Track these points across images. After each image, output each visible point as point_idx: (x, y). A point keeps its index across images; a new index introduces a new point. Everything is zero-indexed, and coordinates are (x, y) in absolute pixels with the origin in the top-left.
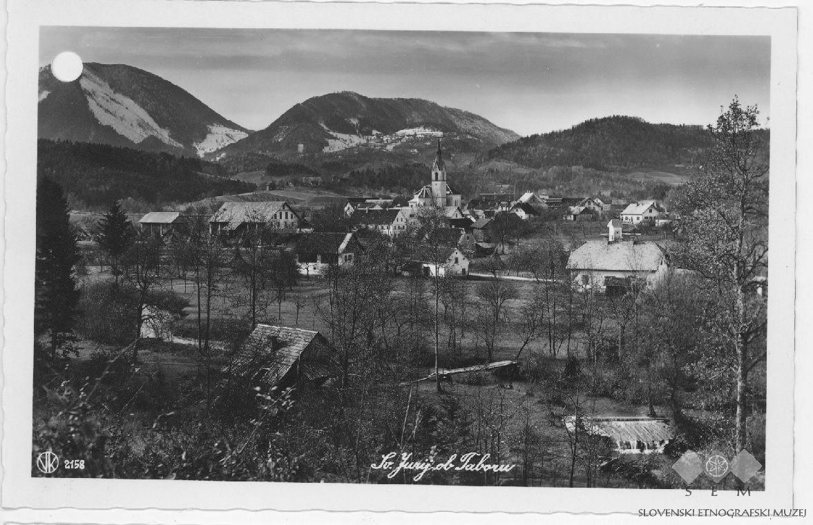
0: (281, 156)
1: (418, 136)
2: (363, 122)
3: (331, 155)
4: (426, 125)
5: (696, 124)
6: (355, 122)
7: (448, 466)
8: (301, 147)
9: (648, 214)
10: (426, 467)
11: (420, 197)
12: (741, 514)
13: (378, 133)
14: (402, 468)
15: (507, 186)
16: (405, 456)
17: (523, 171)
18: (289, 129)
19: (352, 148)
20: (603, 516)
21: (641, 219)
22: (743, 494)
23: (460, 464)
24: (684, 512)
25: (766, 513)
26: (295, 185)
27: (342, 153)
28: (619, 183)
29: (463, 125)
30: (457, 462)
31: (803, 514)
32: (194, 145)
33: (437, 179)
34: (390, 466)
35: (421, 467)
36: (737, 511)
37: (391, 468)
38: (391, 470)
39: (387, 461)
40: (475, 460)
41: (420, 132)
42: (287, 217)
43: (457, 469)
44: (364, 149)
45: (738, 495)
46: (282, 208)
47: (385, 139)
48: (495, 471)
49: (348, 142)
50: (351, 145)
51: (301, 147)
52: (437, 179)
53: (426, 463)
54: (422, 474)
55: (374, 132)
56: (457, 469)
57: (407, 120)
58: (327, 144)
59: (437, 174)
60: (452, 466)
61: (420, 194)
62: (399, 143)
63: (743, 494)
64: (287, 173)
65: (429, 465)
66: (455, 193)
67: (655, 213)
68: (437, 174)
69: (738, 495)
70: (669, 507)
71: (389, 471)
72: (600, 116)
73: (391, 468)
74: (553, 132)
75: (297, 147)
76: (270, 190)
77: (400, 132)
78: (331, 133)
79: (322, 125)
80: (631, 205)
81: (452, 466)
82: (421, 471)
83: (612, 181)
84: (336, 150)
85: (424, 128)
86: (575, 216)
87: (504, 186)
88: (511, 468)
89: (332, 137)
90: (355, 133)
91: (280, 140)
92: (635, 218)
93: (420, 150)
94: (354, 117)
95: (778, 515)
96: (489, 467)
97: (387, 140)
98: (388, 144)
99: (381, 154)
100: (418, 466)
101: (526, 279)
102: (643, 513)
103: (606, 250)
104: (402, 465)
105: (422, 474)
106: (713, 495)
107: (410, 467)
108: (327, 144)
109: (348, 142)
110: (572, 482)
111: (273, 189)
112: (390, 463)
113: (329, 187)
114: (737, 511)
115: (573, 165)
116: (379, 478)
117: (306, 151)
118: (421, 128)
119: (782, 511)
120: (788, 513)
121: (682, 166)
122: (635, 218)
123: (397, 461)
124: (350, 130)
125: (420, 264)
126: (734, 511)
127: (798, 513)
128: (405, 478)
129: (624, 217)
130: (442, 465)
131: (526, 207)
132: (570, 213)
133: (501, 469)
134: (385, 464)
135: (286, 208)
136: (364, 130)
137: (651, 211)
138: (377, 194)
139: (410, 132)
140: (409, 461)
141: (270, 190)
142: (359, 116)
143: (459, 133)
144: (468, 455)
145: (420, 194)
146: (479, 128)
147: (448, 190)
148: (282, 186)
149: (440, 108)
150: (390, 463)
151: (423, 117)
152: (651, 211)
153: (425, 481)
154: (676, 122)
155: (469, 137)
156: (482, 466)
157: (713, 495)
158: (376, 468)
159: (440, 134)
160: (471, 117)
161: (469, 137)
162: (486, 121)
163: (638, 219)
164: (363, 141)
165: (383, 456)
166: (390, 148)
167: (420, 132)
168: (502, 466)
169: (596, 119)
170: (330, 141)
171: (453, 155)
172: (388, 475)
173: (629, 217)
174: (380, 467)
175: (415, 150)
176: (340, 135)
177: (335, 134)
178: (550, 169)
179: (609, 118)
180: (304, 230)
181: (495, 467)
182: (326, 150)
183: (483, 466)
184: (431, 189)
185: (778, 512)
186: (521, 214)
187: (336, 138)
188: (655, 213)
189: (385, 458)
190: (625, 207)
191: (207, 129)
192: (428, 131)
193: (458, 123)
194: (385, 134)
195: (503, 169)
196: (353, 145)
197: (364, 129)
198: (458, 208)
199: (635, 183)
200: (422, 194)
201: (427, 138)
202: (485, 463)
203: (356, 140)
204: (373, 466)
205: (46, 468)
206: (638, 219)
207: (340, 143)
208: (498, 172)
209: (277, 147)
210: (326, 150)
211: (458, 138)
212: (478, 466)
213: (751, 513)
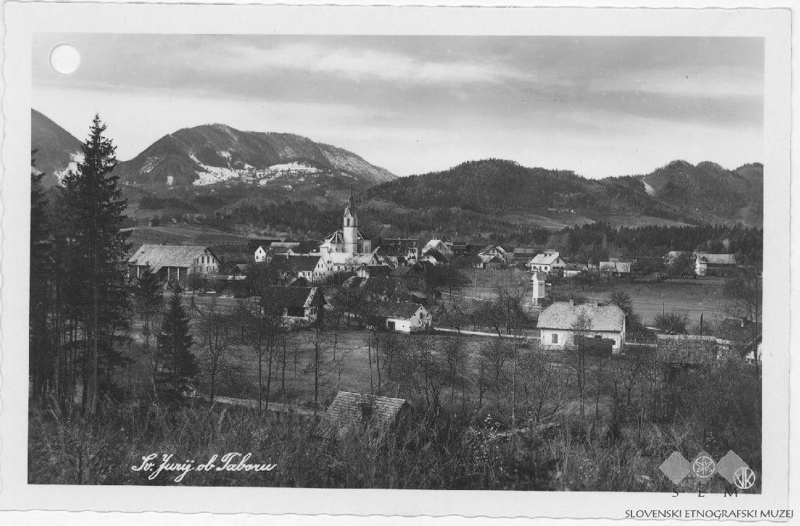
0: (153, 188)
1: (292, 172)
2: (235, 156)
3: (201, 189)
4: (300, 161)
5: (568, 169)
6: (225, 154)
7: (209, 467)
8: (170, 179)
9: (556, 265)
10: (187, 468)
11: (331, 242)
12: (728, 514)
13: (251, 167)
14: (163, 470)
15: (389, 226)
16: (166, 458)
17: (402, 211)
18: (158, 160)
19: (224, 182)
20: (579, 521)
21: (549, 269)
22: (730, 496)
23: (222, 465)
24: (671, 513)
25: (753, 514)
26: (179, 221)
27: (215, 186)
28: (496, 225)
29: (335, 161)
30: (219, 463)
31: (790, 515)
32: (56, 173)
33: (348, 225)
34: (151, 467)
35: (182, 469)
36: (724, 512)
37: (151, 470)
38: (152, 472)
39: (149, 462)
40: (236, 461)
41: (294, 167)
42: (208, 262)
43: (219, 469)
44: (236, 183)
45: (725, 496)
46: (204, 253)
47: (258, 174)
48: (256, 470)
49: (219, 175)
50: (222, 178)
51: (170, 179)
52: (348, 225)
53: (187, 464)
54: (183, 475)
55: (247, 166)
56: (219, 469)
57: (280, 155)
58: (198, 177)
59: (348, 220)
60: (213, 466)
61: (331, 239)
62: (272, 178)
63: (730, 496)
64: (159, 208)
65: (189, 466)
66: (366, 238)
67: (562, 264)
68: (348, 220)
69: (725, 496)
70: (656, 508)
71: (149, 473)
72: (477, 159)
73: (151, 470)
74: (431, 173)
75: (167, 179)
76: (153, 226)
77: (273, 168)
78: (202, 166)
79: (192, 157)
80: (538, 255)
81: (213, 466)
82: (181, 472)
83: (490, 223)
84: (207, 183)
85: (299, 164)
86: (485, 264)
87: (385, 226)
88: (273, 467)
89: (202, 170)
90: (226, 166)
91: (148, 171)
92: (543, 267)
93: (294, 186)
94: (226, 150)
95: (765, 516)
96: (251, 467)
97: (260, 175)
98: (261, 179)
99: (254, 188)
100: (178, 467)
101: (487, 334)
102: (630, 514)
103: (572, 311)
104: (162, 467)
105: (183, 475)
106: (700, 496)
107: (171, 468)
108: (198, 177)
109: (219, 175)
110: (487, 486)
111: (156, 225)
112: (151, 465)
113: (214, 224)
114: (724, 512)
115: (451, 207)
116: (142, 479)
117: (176, 183)
118: (295, 164)
119: (769, 512)
120: (774, 514)
121: (555, 209)
122: (543, 267)
123: (157, 462)
124: (221, 163)
125: (386, 318)
126: (721, 512)
127: (785, 514)
128: (165, 479)
129: (532, 266)
130: (203, 466)
131: (433, 252)
132: (480, 260)
133: (262, 468)
134: (146, 464)
135: (209, 253)
136: (234, 164)
137: (558, 262)
138: (262, 232)
139: (285, 167)
140: (171, 461)
141: (153, 226)
142: (231, 149)
143: (334, 170)
144: (230, 454)
145: (331, 239)
146: (353, 167)
147: (359, 236)
148: (166, 221)
149: (314, 144)
150: (151, 465)
151: (297, 152)
152: (558, 262)
153: (186, 482)
154: (549, 166)
155: (343, 174)
156: (244, 466)
157: (700, 496)
158: (138, 470)
159: (313, 170)
160: (344, 154)
161: (343, 174)
162: (359, 158)
163: (546, 268)
164: (235, 174)
165: (144, 458)
166: (263, 183)
167: (294, 167)
168: (264, 465)
169: (473, 162)
170: (202, 175)
171: (328, 192)
172: (175, 480)
173: (538, 266)
174: (141, 468)
175: (290, 187)
176: (210, 168)
177: (205, 167)
178: (429, 210)
179: (485, 161)
180: (237, 278)
181: (256, 466)
182: (197, 183)
183: (243, 466)
184: (342, 234)
185: (765, 513)
186: (433, 260)
187: (207, 171)
188: (562, 264)
189: (146, 459)
190: (534, 255)
191: (69, 158)
192: (302, 167)
193: (332, 160)
194: (258, 169)
195: (383, 209)
196: (225, 178)
197: (236, 163)
198: (375, 255)
199: (511, 226)
200: (334, 239)
201: (301, 174)
202: (247, 463)
203: (227, 174)
204: (134, 468)
205: (742, 485)
206: (546, 268)
207: (211, 176)
208: (378, 211)
209: (145, 178)
210: (197, 183)
211: (332, 175)
212: (239, 466)
213: (738, 514)
